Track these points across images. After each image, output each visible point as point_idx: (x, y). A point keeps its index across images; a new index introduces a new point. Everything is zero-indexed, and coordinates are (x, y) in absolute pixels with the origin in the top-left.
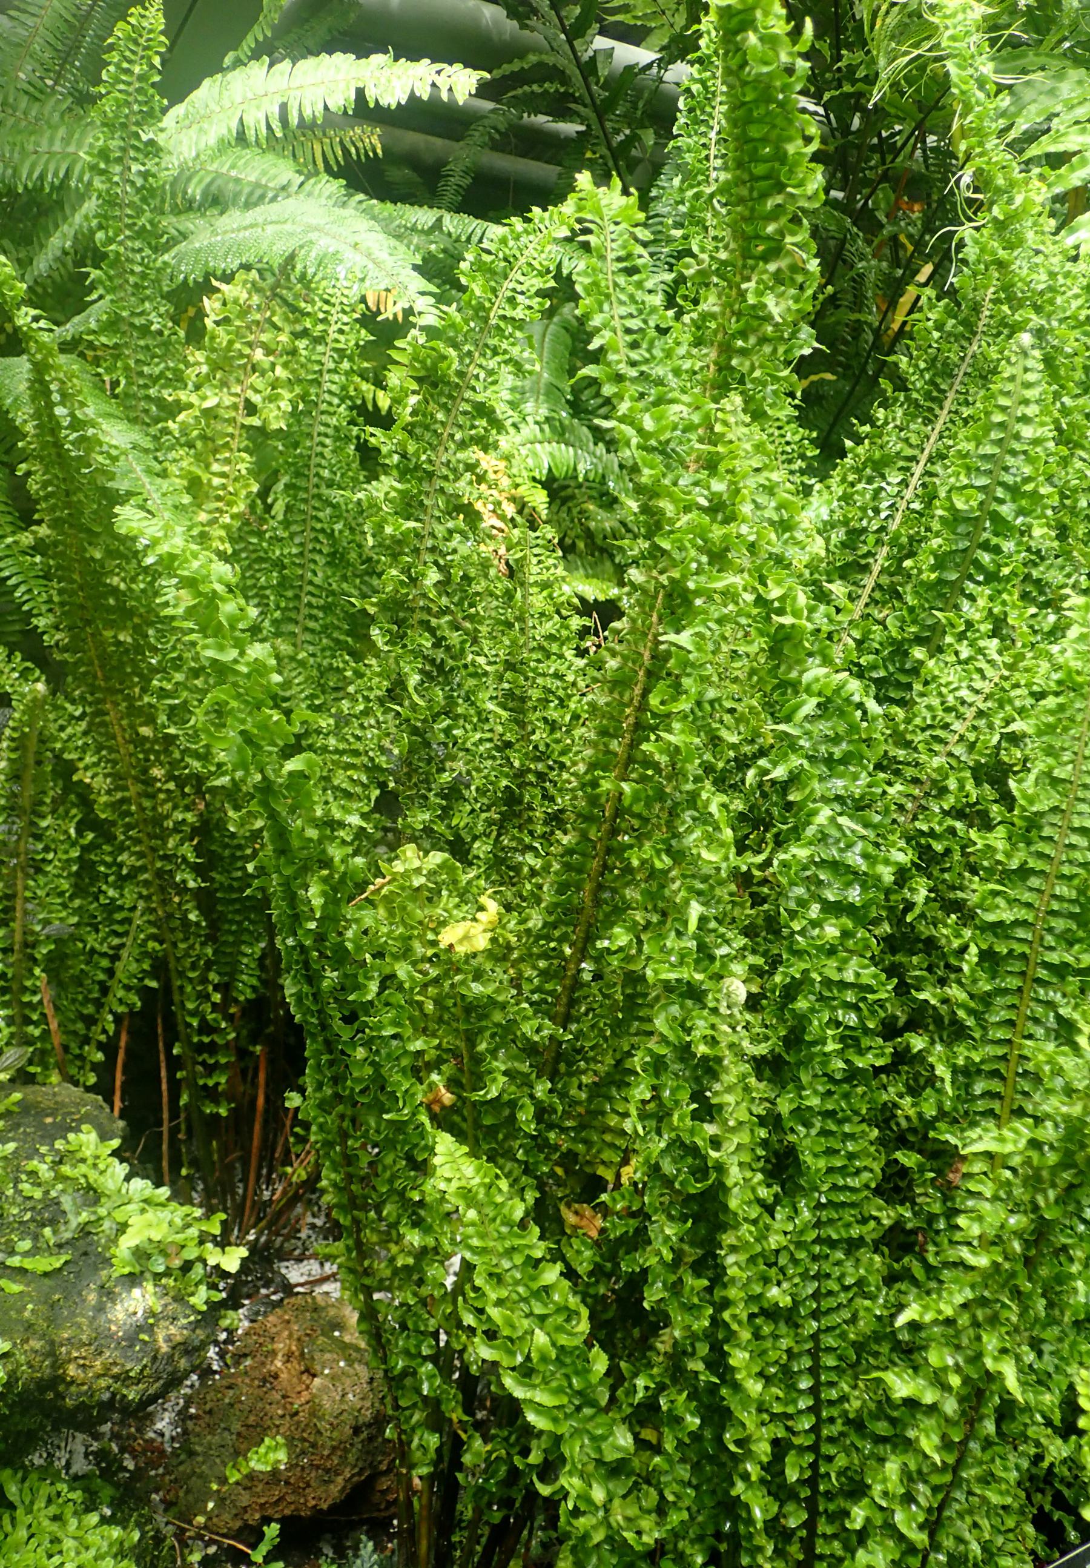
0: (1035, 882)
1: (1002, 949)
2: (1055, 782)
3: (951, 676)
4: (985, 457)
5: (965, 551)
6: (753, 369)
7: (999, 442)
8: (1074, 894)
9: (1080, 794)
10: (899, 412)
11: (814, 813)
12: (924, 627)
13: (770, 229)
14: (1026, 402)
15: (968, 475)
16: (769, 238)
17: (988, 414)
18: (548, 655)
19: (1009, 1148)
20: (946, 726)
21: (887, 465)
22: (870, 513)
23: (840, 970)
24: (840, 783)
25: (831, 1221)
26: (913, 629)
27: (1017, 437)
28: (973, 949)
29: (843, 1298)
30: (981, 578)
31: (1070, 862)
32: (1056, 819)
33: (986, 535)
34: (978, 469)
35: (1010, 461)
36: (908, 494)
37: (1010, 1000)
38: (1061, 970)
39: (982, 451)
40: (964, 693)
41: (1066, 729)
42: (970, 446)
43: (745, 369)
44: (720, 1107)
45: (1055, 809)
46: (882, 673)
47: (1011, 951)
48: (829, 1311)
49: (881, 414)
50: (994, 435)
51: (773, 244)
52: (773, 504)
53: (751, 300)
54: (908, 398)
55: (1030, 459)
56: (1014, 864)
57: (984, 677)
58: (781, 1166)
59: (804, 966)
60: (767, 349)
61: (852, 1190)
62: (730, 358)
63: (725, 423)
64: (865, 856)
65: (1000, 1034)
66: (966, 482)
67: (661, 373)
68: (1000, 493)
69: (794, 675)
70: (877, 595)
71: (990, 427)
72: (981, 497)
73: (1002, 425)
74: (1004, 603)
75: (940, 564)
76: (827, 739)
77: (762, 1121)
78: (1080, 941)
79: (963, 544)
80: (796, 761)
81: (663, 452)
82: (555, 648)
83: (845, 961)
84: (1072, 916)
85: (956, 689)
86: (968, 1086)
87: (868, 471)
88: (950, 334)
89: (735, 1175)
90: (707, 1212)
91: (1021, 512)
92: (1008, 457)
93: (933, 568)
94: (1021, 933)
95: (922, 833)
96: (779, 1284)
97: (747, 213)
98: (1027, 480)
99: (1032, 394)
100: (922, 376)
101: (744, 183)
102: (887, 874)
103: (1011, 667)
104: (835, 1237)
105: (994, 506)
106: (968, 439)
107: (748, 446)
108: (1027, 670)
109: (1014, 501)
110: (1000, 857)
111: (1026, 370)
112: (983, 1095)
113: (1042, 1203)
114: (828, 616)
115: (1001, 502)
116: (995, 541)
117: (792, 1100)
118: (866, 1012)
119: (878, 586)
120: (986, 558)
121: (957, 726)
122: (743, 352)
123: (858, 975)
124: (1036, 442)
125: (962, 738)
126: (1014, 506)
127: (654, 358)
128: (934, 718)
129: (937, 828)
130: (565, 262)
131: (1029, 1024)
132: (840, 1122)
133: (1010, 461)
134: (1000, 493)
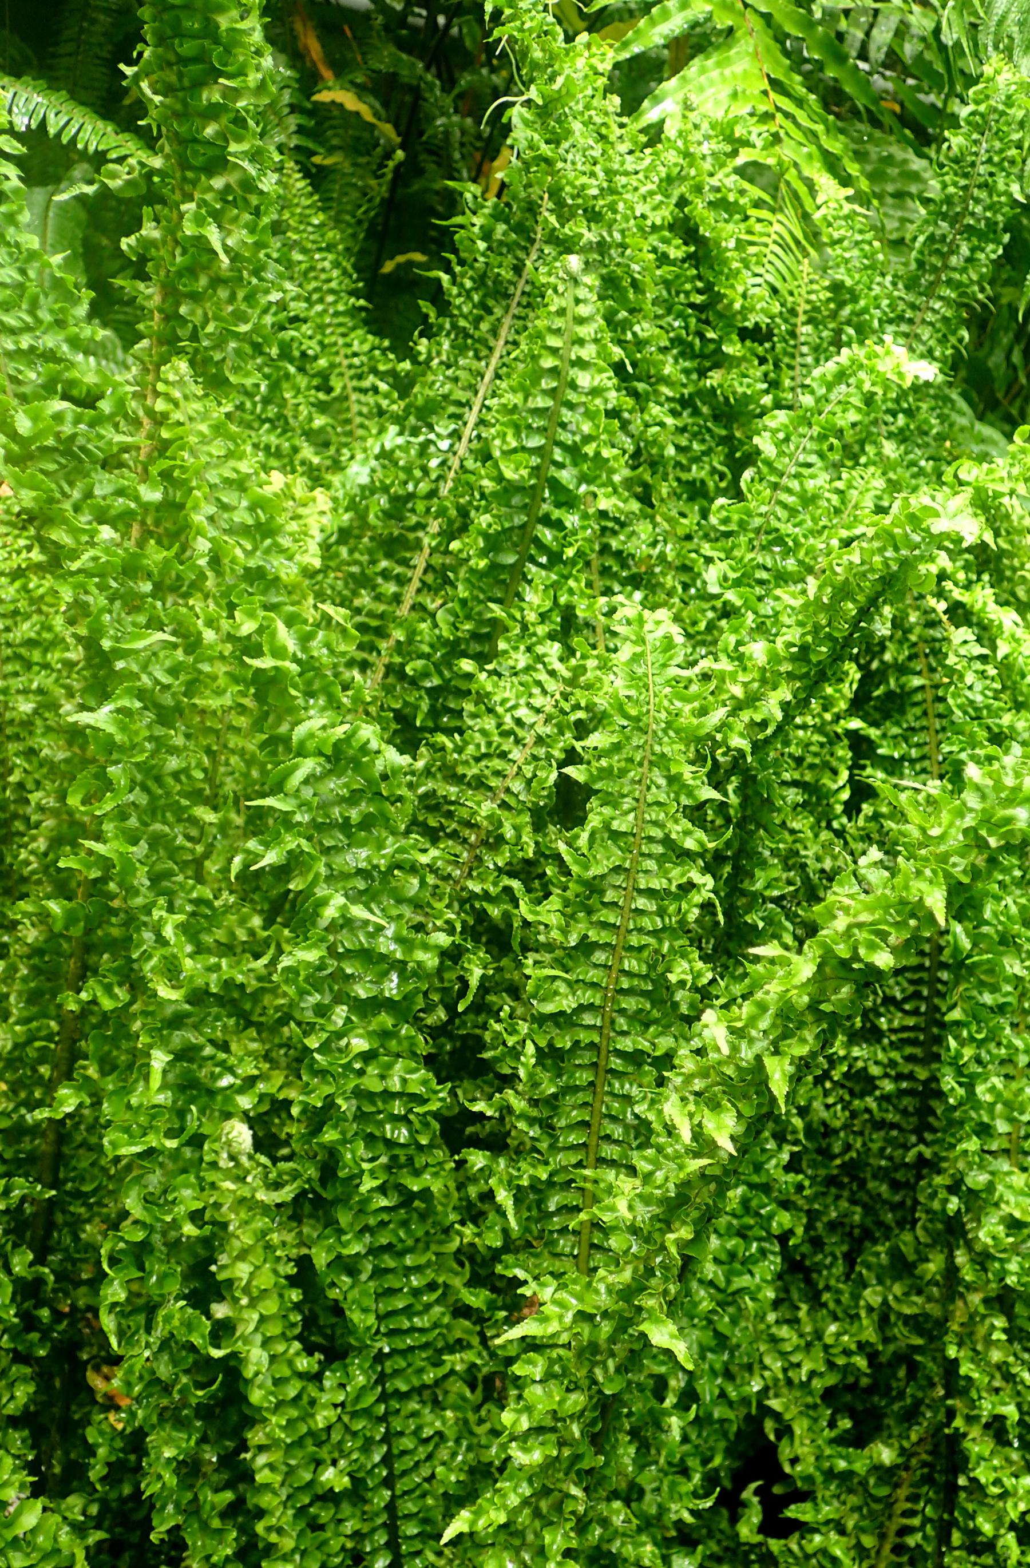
0: (599, 957)
1: (565, 1043)
2: (616, 835)
3: (504, 691)
4: (537, 412)
5: (523, 526)
6: (206, 321)
7: (552, 393)
8: (644, 970)
9: (645, 849)
10: (446, 345)
11: (324, 902)
12: (482, 622)
13: (210, 131)
14: (580, 342)
15: (517, 435)
16: (208, 143)
17: (535, 358)
18: (28, 665)
19: (553, 1327)
20: (503, 755)
21: (434, 412)
22: (418, 473)
23: (383, 1077)
24: (364, 853)
25: (397, 1373)
26: (467, 626)
27: (573, 386)
28: (530, 1049)
29: (422, 1452)
30: (544, 560)
31: (640, 930)
32: (619, 880)
33: (545, 507)
34: (529, 427)
35: (567, 415)
36: (462, 448)
37: (581, 1097)
38: (636, 1058)
39: (531, 404)
40: (522, 713)
41: (623, 773)
42: (517, 399)
43: (198, 318)
44: (230, 1282)
45: (617, 869)
46: (436, 681)
47: (576, 1043)
48: (404, 1473)
49: (423, 346)
50: (547, 383)
51: (211, 152)
52: (245, 503)
53: (189, 229)
54: (454, 326)
55: (590, 415)
56: (573, 940)
57: (545, 692)
58: (324, 1333)
59: (328, 1090)
60: (223, 294)
61: (421, 1330)
62: (178, 305)
63: (168, 398)
64: (399, 940)
65: (573, 1139)
66: (514, 444)
67: (50, 344)
68: (558, 455)
69: (284, 729)
70: (430, 578)
71: (538, 374)
72: (535, 461)
73: (554, 372)
74: (571, 592)
75: (493, 543)
76: (342, 800)
77: (293, 1281)
78: (656, 1022)
79: (520, 519)
80: (292, 842)
81: (68, 453)
82: (36, 656)
83: (389, 1066)
84: (644, 994)
85: (514, 707)
86: (540, 1203)
87: (412, 420)
88: (501, 243)
89: (256, 1358)
90: (227, 1409)
91: (583, 479)
92: (564, 410)
93: (483, 553)
94: (588, 1019)
95: (474, 896)
96: (334, 1463)
97: (178, 107)
98: (587, 439)
99: (585, 331)
100: (469, 297)
101: (170, 64)
102: (430, 960)
103: (572, 682)
104: (404, 1388)
105: (553, 472)
106: (514, 390)
107: (204, 428)
108: (588, 687)
109: (575, 464)
110: (555, 934)
111: (578, 301)
112: (559, 1211)
113: (600, 1379)
114: (328, 645)
115: (561, 466)
116: (556, 514)
117: (329, 1249)
118: (417, 1125)
119: (429, 568)
120: (547, 535)
121: (516, 754)
122: (195, 297)
123: (404, 1081)
124: (595, 392)
125: (519, 772)
126: (575, 472)
127: (39, 321)
128: (489, 744)
129: (492, 889)
130: (51, 117)
131: (606, 1122)
132: (401, 1254)
133: (567, 415)
134: (558, 455)
